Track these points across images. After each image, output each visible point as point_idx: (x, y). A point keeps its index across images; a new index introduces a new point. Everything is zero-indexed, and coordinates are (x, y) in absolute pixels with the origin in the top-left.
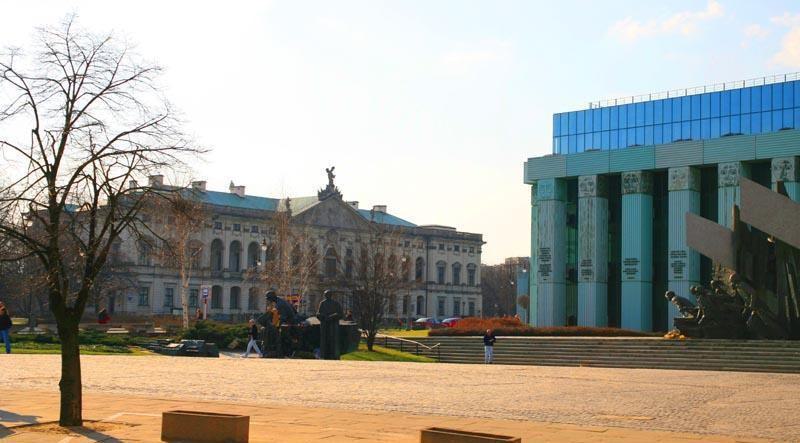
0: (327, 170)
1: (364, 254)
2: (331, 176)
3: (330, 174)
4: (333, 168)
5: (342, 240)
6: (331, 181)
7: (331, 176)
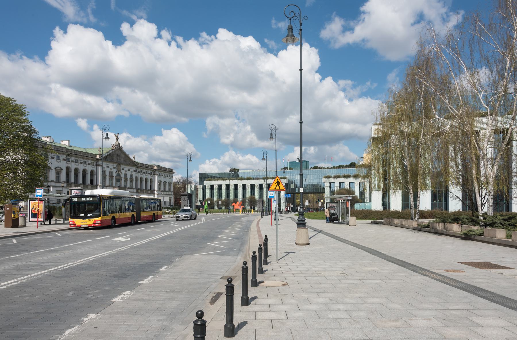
1: (132, 175)
5: (123, 169)
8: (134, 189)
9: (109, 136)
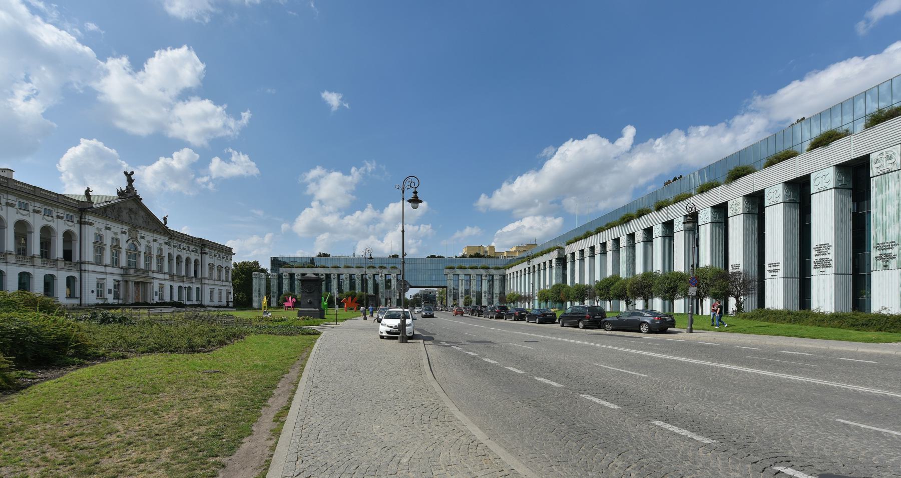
0: (126, 173)
2: (130, 181)
7: (130, 181)
9: (125, 178)
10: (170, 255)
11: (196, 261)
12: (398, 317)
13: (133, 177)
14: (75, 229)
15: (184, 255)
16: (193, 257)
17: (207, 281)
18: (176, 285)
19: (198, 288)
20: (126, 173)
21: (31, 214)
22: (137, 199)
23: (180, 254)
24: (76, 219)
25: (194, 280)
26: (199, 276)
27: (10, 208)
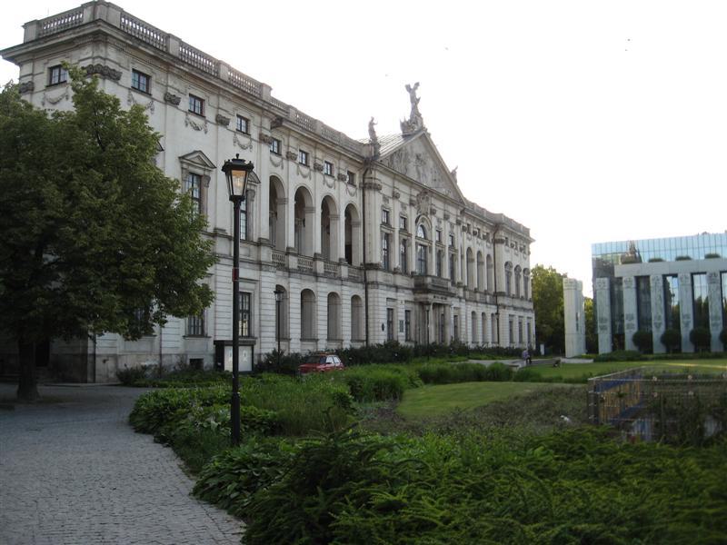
0: (408, 88)
2: (415, 101)
3: (411, 90)
4: (417, 84)
6: (415, 108)
7: (415, 101)
8: (395, 272)
9: (407, 96)
10: (275, 183)
11: (350, 210)
12: (75, 227)
13: (418, 94)
14: (357, 201)
15: (319, 189)
16: (344, 196)
17: (380, 276)
18: (295, 287)
19: (355, 298)
20: (408, 88)
21: (211, 127)
22: (425, 138)
23: (308, 183)
24: (357, 181)
25: (344, 271)
26: (358, 259)
27: (221, 129)
